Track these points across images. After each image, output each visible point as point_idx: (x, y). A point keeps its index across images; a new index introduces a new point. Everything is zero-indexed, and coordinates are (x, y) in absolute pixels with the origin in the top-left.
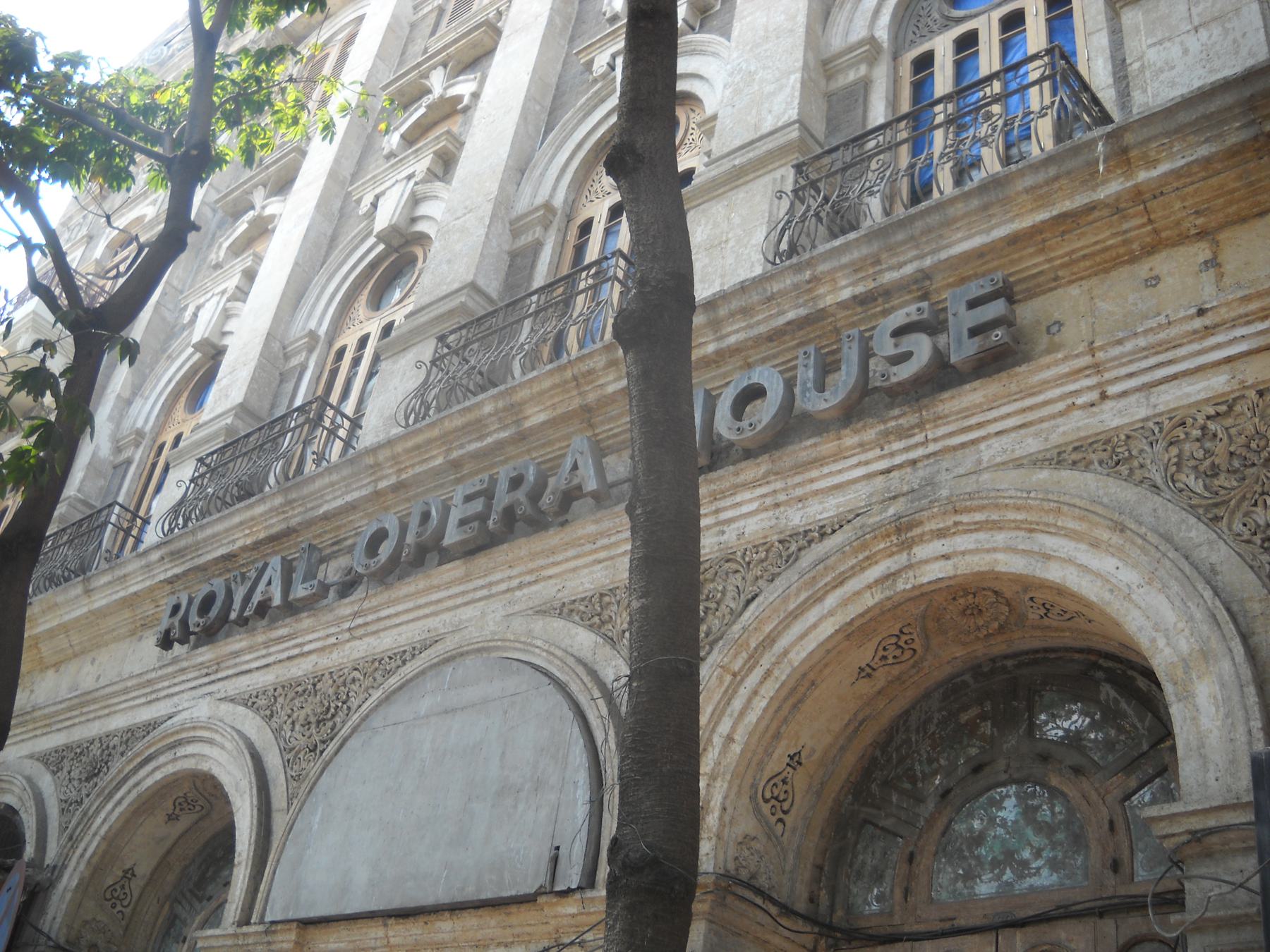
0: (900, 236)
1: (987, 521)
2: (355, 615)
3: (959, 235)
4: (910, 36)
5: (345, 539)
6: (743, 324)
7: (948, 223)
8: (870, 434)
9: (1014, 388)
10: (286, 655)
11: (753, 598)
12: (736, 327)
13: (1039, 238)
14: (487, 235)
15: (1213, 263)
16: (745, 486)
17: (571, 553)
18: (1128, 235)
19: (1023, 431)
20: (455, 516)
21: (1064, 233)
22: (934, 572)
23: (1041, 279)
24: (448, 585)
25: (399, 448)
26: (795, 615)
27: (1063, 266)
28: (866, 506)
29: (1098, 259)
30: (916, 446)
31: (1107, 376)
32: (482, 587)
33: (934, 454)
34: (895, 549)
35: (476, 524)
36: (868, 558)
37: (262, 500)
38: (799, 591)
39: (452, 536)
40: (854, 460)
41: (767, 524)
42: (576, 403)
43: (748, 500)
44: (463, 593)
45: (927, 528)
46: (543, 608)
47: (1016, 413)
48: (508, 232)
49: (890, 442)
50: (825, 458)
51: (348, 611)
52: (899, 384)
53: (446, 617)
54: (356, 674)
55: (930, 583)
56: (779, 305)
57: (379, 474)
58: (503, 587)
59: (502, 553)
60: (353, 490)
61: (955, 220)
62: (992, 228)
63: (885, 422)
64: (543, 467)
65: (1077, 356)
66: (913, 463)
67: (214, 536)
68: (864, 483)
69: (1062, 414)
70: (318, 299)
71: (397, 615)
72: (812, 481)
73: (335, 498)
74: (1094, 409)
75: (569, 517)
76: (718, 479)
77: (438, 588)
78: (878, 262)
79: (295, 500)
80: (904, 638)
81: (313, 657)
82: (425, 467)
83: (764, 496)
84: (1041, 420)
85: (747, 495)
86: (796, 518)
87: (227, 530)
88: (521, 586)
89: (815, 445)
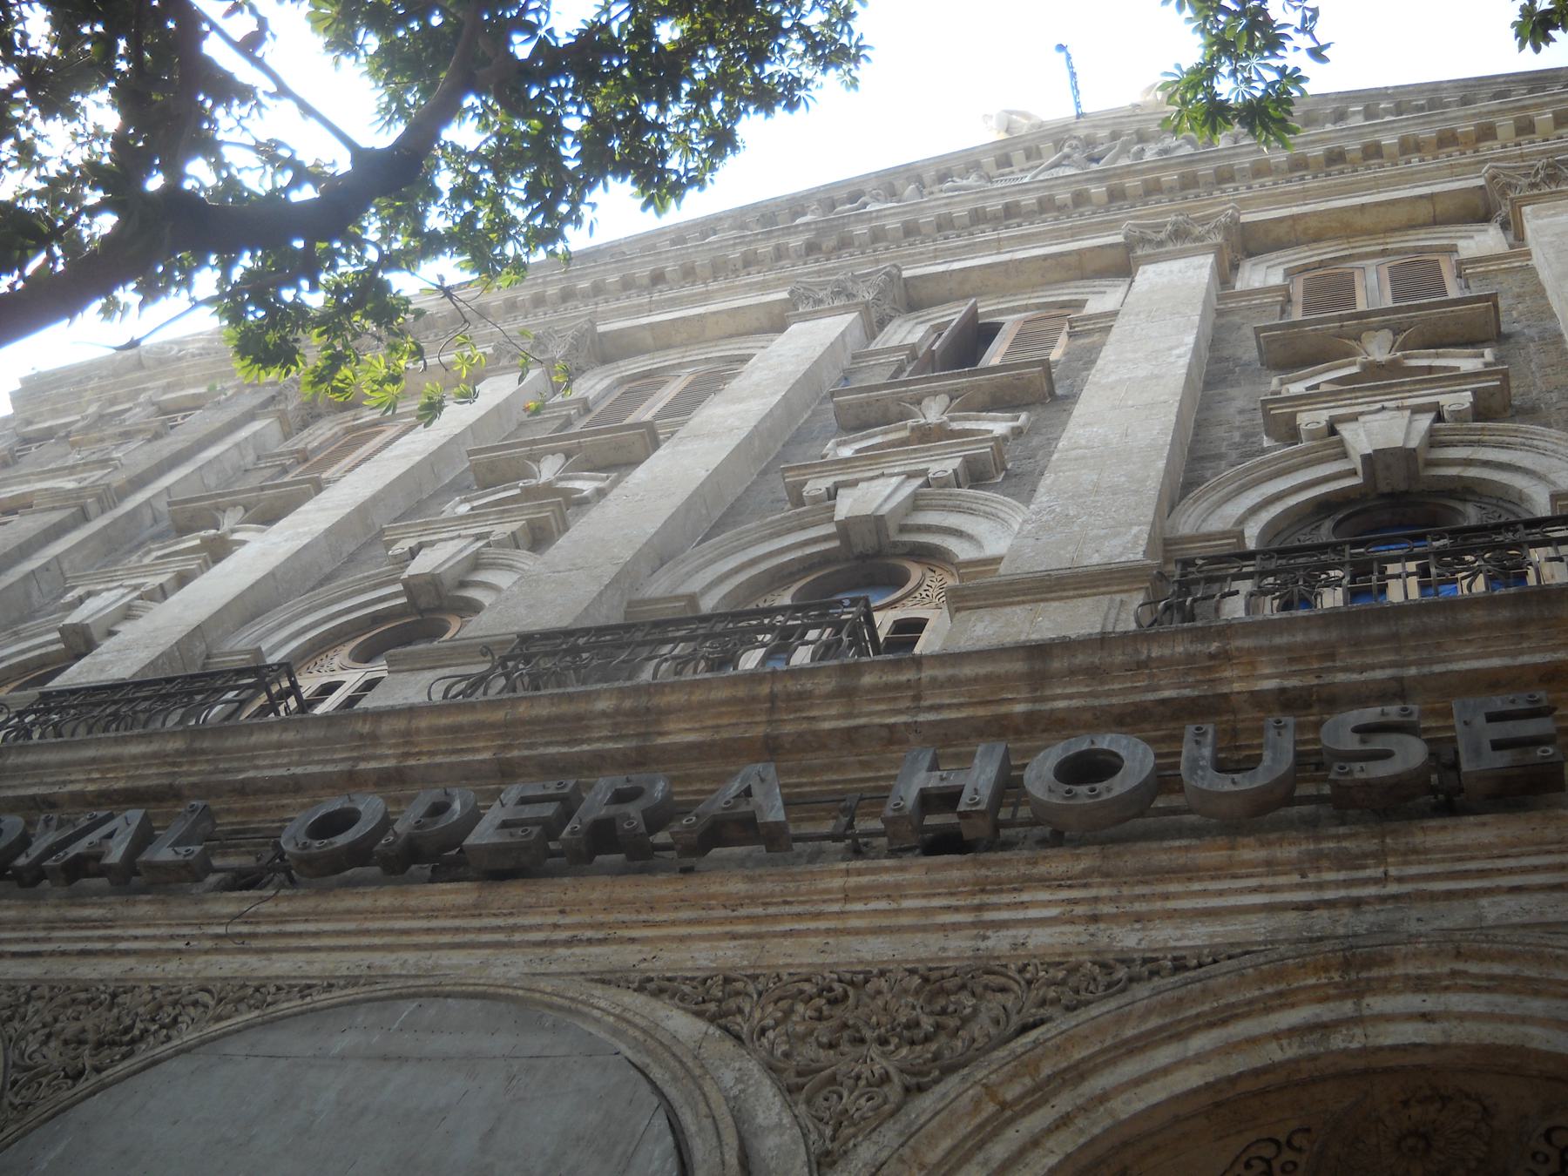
0: (1377, 630)
1: (1514, 978)
8: (1288, 852)
10: (80, 946)
11: (1035, 1026)
12: (1069, 691)
14: (601, 594)
16: (1045, 882)
17: (685, 914)
19: (1557, 895)
20: (493, 816)
24: (433, 913)
25: (423, 723)
26: (1131, 1048)
28: (1265, 943)
30: (1365, 882)
32: (498, 929)
33: (1395, 897)
34: (1332, 992)
35: (536, 830)
36: (1280, 994)
37: (147, 737)
38: (1149, 1011)
41: (1072, 939)
42: (760, 731)
43: (1042, 902)
44: (457, 930)
45: (1399, 970)
46: (608, 977)
49: (1319, 870)
50: (1199, 869)
51: (232, 909)
52: (1367, 785)
53: (411, 957)
54: (206, 997)
55: (1394, 1048)
56: (1151, 676)
57: (369, 751)
59: (550, 890)
60: (310, 763)
62: (1522, 652)
63: (1318, 839)
66: (1356, 904)
67: (36, 766)
68: (1263, 915)
70: (281, 626)
71: (316, 934)
72: (1166, 897)
73: (273, 766)
76: (997, 863)
77: (414, 913)
78: (1332, 656)
79: (203, 752)
80: (1288, 1155)
81: (130, 962)
82: (454, 758)
83: (1075, 902)
85: (1044, 895)
86: (1128, 939)
87: (63, 765)
88: (569, 943)
89: (1187, 848)
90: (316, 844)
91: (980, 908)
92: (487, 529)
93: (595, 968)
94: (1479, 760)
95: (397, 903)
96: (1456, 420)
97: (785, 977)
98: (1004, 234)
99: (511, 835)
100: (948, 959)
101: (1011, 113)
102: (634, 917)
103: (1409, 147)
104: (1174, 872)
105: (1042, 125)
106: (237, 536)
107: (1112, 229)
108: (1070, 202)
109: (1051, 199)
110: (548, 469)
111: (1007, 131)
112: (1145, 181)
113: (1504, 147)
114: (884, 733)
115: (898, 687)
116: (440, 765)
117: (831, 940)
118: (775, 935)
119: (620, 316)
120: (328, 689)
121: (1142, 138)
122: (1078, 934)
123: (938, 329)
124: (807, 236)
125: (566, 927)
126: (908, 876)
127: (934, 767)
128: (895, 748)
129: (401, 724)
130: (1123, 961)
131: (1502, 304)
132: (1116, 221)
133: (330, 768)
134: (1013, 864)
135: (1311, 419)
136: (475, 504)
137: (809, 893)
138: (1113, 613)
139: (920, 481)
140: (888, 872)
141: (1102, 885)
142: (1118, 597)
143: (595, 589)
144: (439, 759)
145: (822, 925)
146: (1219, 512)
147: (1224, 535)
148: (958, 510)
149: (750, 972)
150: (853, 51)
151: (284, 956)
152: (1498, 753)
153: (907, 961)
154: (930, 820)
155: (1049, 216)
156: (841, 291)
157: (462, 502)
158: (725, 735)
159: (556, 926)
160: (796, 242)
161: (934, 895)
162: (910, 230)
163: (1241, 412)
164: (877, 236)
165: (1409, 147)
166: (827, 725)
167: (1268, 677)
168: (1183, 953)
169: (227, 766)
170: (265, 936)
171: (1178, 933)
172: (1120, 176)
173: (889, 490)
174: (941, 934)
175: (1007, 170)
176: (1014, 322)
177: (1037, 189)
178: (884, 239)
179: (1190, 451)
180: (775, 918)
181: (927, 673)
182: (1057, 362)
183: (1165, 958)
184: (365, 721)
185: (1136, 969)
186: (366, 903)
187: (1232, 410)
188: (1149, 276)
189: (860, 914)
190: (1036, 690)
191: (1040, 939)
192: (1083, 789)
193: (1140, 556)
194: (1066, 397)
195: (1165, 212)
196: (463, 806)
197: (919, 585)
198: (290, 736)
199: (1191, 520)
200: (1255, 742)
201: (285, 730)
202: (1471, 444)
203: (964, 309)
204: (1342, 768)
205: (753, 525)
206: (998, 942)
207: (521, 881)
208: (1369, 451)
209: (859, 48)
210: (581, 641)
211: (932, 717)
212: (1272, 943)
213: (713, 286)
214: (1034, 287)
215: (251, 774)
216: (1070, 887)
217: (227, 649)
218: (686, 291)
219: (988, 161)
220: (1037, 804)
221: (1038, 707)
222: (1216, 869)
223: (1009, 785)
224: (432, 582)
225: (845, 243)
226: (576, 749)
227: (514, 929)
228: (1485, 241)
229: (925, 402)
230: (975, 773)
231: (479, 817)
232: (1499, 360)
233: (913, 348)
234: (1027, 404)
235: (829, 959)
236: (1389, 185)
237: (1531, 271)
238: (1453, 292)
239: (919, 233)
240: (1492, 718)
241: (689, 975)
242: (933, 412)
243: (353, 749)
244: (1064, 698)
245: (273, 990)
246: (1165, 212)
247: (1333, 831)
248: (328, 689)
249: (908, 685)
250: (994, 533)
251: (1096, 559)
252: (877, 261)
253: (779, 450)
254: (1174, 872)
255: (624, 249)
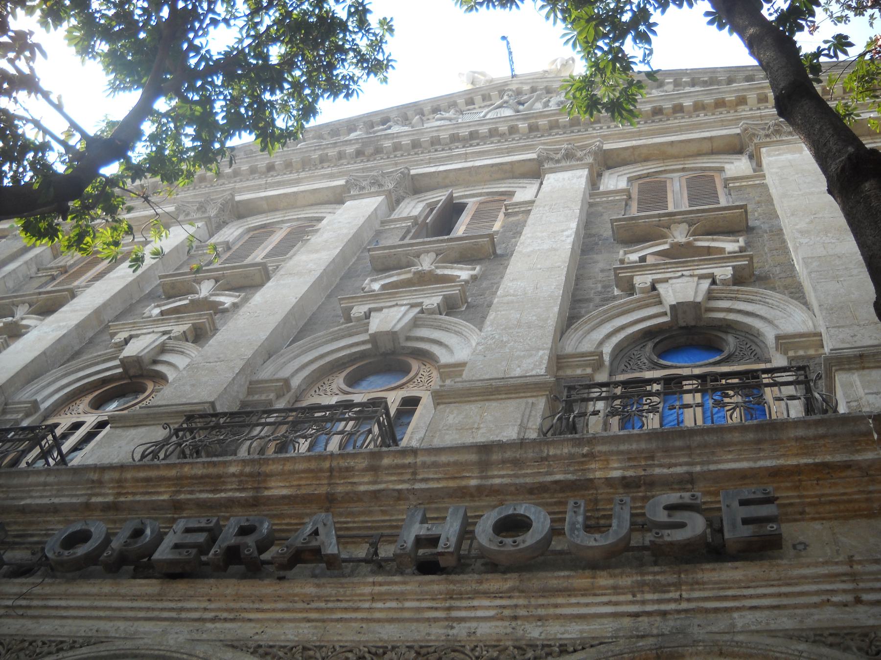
0: (679, 443)
2: (21, 596)
3: (730, 457)
4: (623, 367)
5: (32, 536)
6: (512, 473)
7: (723, 445)
8: (626, 581)
9: (773, 574)
12: (502, 473)
13: (797, 478)
14: (234, 379)
16: (486, 594)
18: (873, 495)
19: (776, 612)
20: (170, 540)
21: (818, 479)
23: (790, 510)
24: (135, 598)
27: (811, 504)
28: (612, 637)
29: (842, 507)
30: (669, 601)
31: (862, 585)
32: (172, 609)
33: (686, 611)
35: (194, 551)
39: (163, 553)
40: (605, 599)
41: (502, 631)
42: (323, 490)
43: (485, 607)
44: (148, 609)
46: (235, 644)
47: (772, 595)
48: (246, 387)
49: (643, 592)
50: (575, 590)
51: (16, 590)
52: (671, 544)
53: (122, 625)
57: (97, 490)
58: (196, 615)
59: (204, 587)
61: (730, 444)
62: (759, 459)
63: (642, 574)
64: (274, 527)
65: (837, 563)
66: (664, 614)
68: (611, 619)
69: (815, 605)
70: (49, 385)
71: (66, 608)
72: (556, 606)
73: (41, 497)
74: (847, 609)
75: (288, 574)
76: (459, 582)
77: (123, 597)
78: (652, 458)
82: (147, 498)
83: (504, 607)
84: (795, 607)
85: (486, 602)
88: (214, 620)
89: (568, 577)
90: (66, 553)
91: (449, 609)
92: (169, 328)
93: (229, 637)
94: (735, 533)
95: (114, 590)
96: (723, 284)
97: (338, 649)
98: (470, 150)
99: (180, 554)
100: (431, 641)
101: (475, 72)
102: (251, 606)
103: (699, 107)
104: (560, 591)
105: (492, 81)
106: (24, 322)
107: (531, 149)
108: (507, 132)
109: (496, 129)
110: (205, 289)
111: (472, 83)
112: (550, 121)
113: (751, 110)
114: (396, 494)
115: (404, 466)
116: (139, 501)
117: (364, 625)
118: (332, 620)
119: (249, 191)
120: (76, 426)
121: (548, 91)
122: (505, 627)
123: (431, 207)
124: (357, 146)
125: (212, 610)
126: (408, 588)
127: (424, 520)
128: (402, 502)
129: (116, 475)
130: (531, 646)
131: (750, 208)
132: (533, 145)
133: (74, 500)
134: (468, 582)
135: (642, 280)
136: (163, 308)
137: (351, 595)
138: (528, 411)
139: (418, 309)
140: (398, 584)
141: (519, 597)
142: (530, 400)
143: (230, 376)
144: (138, 498)
145: (359, 615)
146: (588, 337)
147: (591, 354)
148: (439, 328)
149: (318, 644)
150: (385, 62)
151: (46, 621)
152: (746, 527)
153: (408, 641)
154: (421, 552)
155: (495, 139)
156: (375, 182)
157: (155, 307)
158: (304, 492)
159: (205, 609)
160: (350, 150)
161: (423, 600)
162: (416, 145)
163: (602, 271)
164: (397, 147)
165: (699, 107)
166: (362, 488)
167: (616, 469)
168: (566, 642)
169: (14, 495)
170: (35, 607)
171: (563, 629)
172: (536, 118)
173: (400, 315)
174: (427, 624)
175: (472, 107)
176: (474, 203)
177: (488, 123)
178: (401, 149)
179: (573, 295)
180: (332, 610)
181: (420, 459)
182: (497, 232)
183: (555, 645)
184: (95, 472)
185: (539, 652)
186: (95, 590)
187: (597, 270)
188: (551, 180)
189: (381, 610)
190: (483, 472)
191: (485, 630)
192: (509, 540)
193: (543, 372)
194: (502, 256)
195: (560, 141)
196: (152, 532)
197: (417, 374)
198: (51, 479)
199: (573, 343)
200: (608, 507)
201: (48, 475)
202: (731, 299)
203: (447, 193)
204: (657, 533)
205: (321, 334)
206: (460, 631)
207: (186, 580)
208: (674, 303)
209: (389, 61)
210: (222, 421)
211: (423, 486)
212: (616, 637)
213: (303, 175)
214: (486, 182)
215: (28, 501)
216: (501, 597)
217: (17, 399)
218: (286, 177)
219: (461, 101)
220: (481, 547)
221: (484, 482)
222: (585, 590)
223: (466, 532)
224: (137, 361)
225: (378, 151)
226: (218, 496)
227: (182, 609)
228: (739, 166)
229: (422, 256)
230: (447, 526)
231: (162, 540)
232: (748, 244)
233: (415, 218)
234: (481, 259)
235: (363, 638)
236: (687, 130)
237: (765, 186)
238: (723, 202)
239: (421, 146)
240: (744, 503)
241: (283, 644)
242: (426, 263)
243: (88, 489)
244: (499, 477)
245: (40, 644)
246: (560, 141)
247: (651, 569)
248: (76, 426)
249: (409, 466)
250: (460, 346)
251: (518, 372)
252: (396, 164)
253: (340, 280)
254: (560, 591)
255: (252, 148)
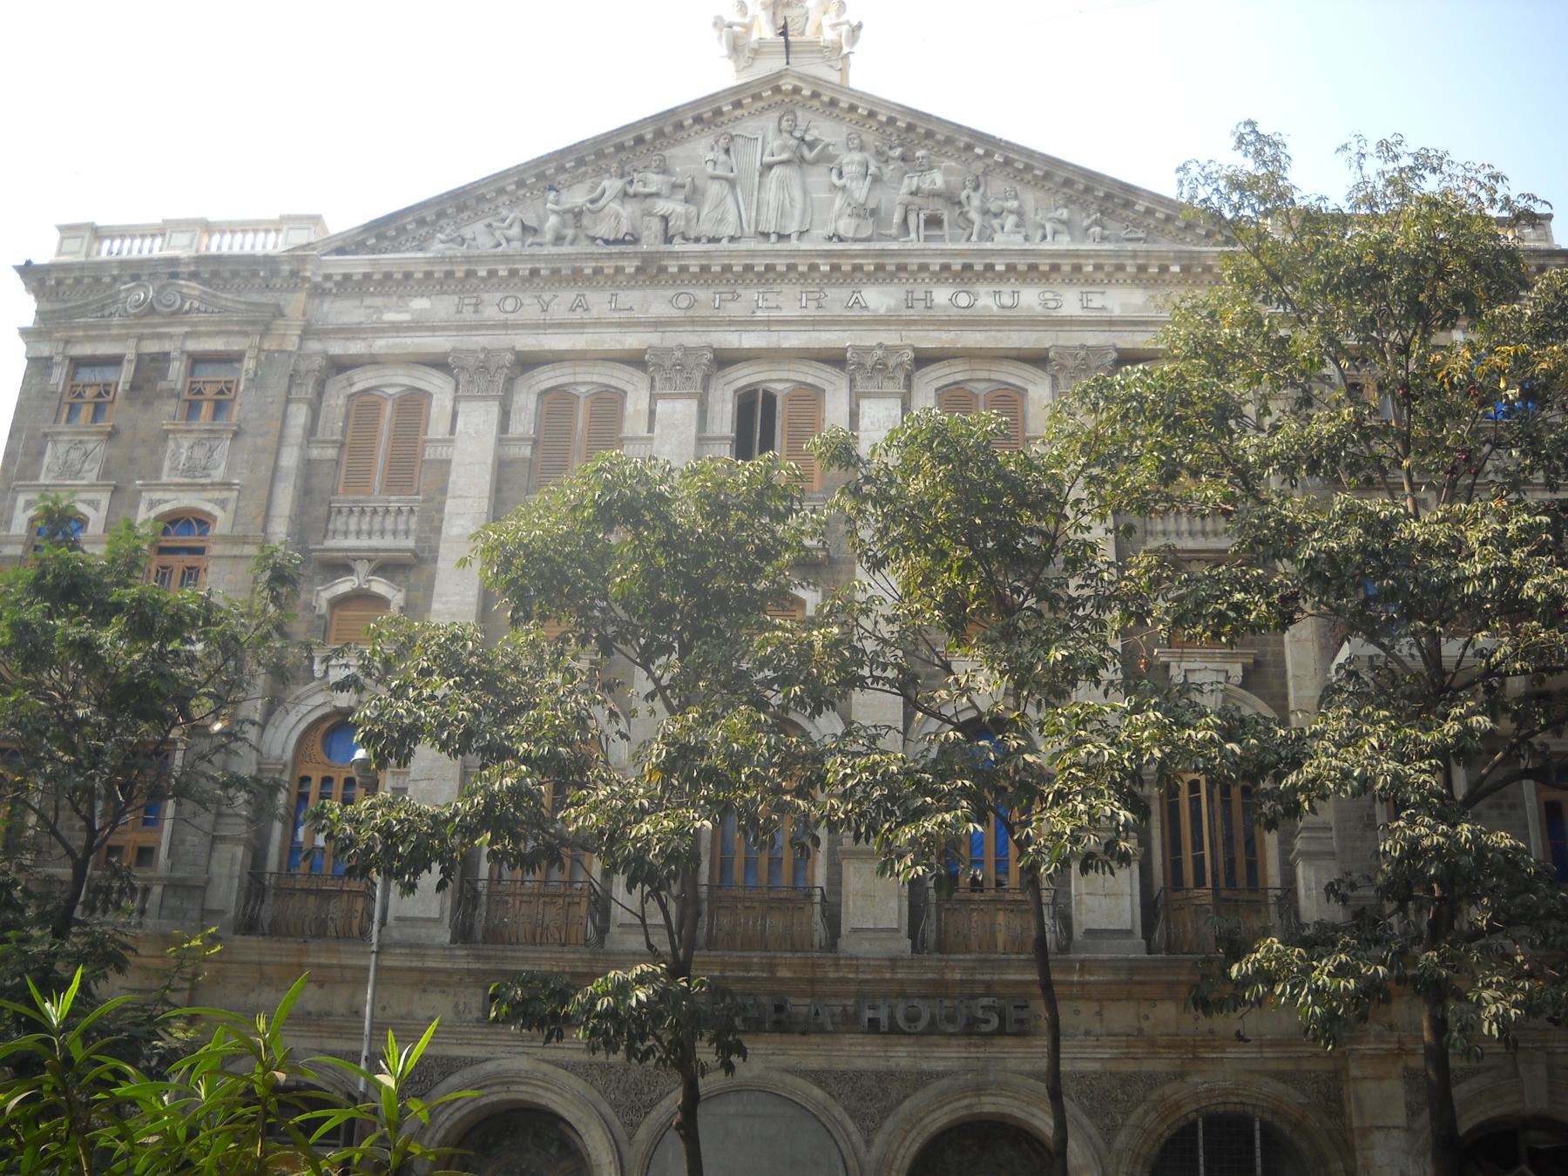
15: (1099, 1014)
22: (988, 1109)
